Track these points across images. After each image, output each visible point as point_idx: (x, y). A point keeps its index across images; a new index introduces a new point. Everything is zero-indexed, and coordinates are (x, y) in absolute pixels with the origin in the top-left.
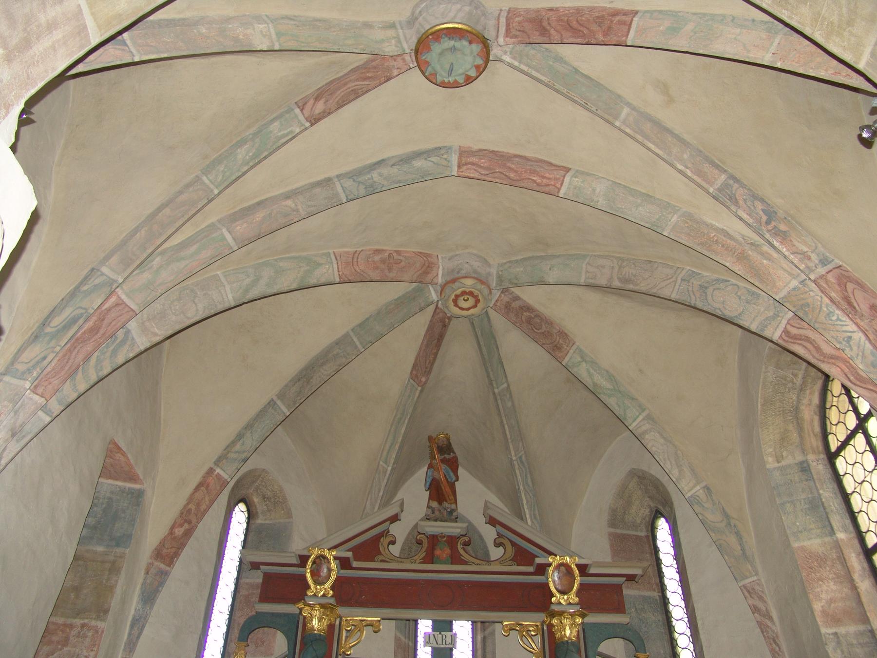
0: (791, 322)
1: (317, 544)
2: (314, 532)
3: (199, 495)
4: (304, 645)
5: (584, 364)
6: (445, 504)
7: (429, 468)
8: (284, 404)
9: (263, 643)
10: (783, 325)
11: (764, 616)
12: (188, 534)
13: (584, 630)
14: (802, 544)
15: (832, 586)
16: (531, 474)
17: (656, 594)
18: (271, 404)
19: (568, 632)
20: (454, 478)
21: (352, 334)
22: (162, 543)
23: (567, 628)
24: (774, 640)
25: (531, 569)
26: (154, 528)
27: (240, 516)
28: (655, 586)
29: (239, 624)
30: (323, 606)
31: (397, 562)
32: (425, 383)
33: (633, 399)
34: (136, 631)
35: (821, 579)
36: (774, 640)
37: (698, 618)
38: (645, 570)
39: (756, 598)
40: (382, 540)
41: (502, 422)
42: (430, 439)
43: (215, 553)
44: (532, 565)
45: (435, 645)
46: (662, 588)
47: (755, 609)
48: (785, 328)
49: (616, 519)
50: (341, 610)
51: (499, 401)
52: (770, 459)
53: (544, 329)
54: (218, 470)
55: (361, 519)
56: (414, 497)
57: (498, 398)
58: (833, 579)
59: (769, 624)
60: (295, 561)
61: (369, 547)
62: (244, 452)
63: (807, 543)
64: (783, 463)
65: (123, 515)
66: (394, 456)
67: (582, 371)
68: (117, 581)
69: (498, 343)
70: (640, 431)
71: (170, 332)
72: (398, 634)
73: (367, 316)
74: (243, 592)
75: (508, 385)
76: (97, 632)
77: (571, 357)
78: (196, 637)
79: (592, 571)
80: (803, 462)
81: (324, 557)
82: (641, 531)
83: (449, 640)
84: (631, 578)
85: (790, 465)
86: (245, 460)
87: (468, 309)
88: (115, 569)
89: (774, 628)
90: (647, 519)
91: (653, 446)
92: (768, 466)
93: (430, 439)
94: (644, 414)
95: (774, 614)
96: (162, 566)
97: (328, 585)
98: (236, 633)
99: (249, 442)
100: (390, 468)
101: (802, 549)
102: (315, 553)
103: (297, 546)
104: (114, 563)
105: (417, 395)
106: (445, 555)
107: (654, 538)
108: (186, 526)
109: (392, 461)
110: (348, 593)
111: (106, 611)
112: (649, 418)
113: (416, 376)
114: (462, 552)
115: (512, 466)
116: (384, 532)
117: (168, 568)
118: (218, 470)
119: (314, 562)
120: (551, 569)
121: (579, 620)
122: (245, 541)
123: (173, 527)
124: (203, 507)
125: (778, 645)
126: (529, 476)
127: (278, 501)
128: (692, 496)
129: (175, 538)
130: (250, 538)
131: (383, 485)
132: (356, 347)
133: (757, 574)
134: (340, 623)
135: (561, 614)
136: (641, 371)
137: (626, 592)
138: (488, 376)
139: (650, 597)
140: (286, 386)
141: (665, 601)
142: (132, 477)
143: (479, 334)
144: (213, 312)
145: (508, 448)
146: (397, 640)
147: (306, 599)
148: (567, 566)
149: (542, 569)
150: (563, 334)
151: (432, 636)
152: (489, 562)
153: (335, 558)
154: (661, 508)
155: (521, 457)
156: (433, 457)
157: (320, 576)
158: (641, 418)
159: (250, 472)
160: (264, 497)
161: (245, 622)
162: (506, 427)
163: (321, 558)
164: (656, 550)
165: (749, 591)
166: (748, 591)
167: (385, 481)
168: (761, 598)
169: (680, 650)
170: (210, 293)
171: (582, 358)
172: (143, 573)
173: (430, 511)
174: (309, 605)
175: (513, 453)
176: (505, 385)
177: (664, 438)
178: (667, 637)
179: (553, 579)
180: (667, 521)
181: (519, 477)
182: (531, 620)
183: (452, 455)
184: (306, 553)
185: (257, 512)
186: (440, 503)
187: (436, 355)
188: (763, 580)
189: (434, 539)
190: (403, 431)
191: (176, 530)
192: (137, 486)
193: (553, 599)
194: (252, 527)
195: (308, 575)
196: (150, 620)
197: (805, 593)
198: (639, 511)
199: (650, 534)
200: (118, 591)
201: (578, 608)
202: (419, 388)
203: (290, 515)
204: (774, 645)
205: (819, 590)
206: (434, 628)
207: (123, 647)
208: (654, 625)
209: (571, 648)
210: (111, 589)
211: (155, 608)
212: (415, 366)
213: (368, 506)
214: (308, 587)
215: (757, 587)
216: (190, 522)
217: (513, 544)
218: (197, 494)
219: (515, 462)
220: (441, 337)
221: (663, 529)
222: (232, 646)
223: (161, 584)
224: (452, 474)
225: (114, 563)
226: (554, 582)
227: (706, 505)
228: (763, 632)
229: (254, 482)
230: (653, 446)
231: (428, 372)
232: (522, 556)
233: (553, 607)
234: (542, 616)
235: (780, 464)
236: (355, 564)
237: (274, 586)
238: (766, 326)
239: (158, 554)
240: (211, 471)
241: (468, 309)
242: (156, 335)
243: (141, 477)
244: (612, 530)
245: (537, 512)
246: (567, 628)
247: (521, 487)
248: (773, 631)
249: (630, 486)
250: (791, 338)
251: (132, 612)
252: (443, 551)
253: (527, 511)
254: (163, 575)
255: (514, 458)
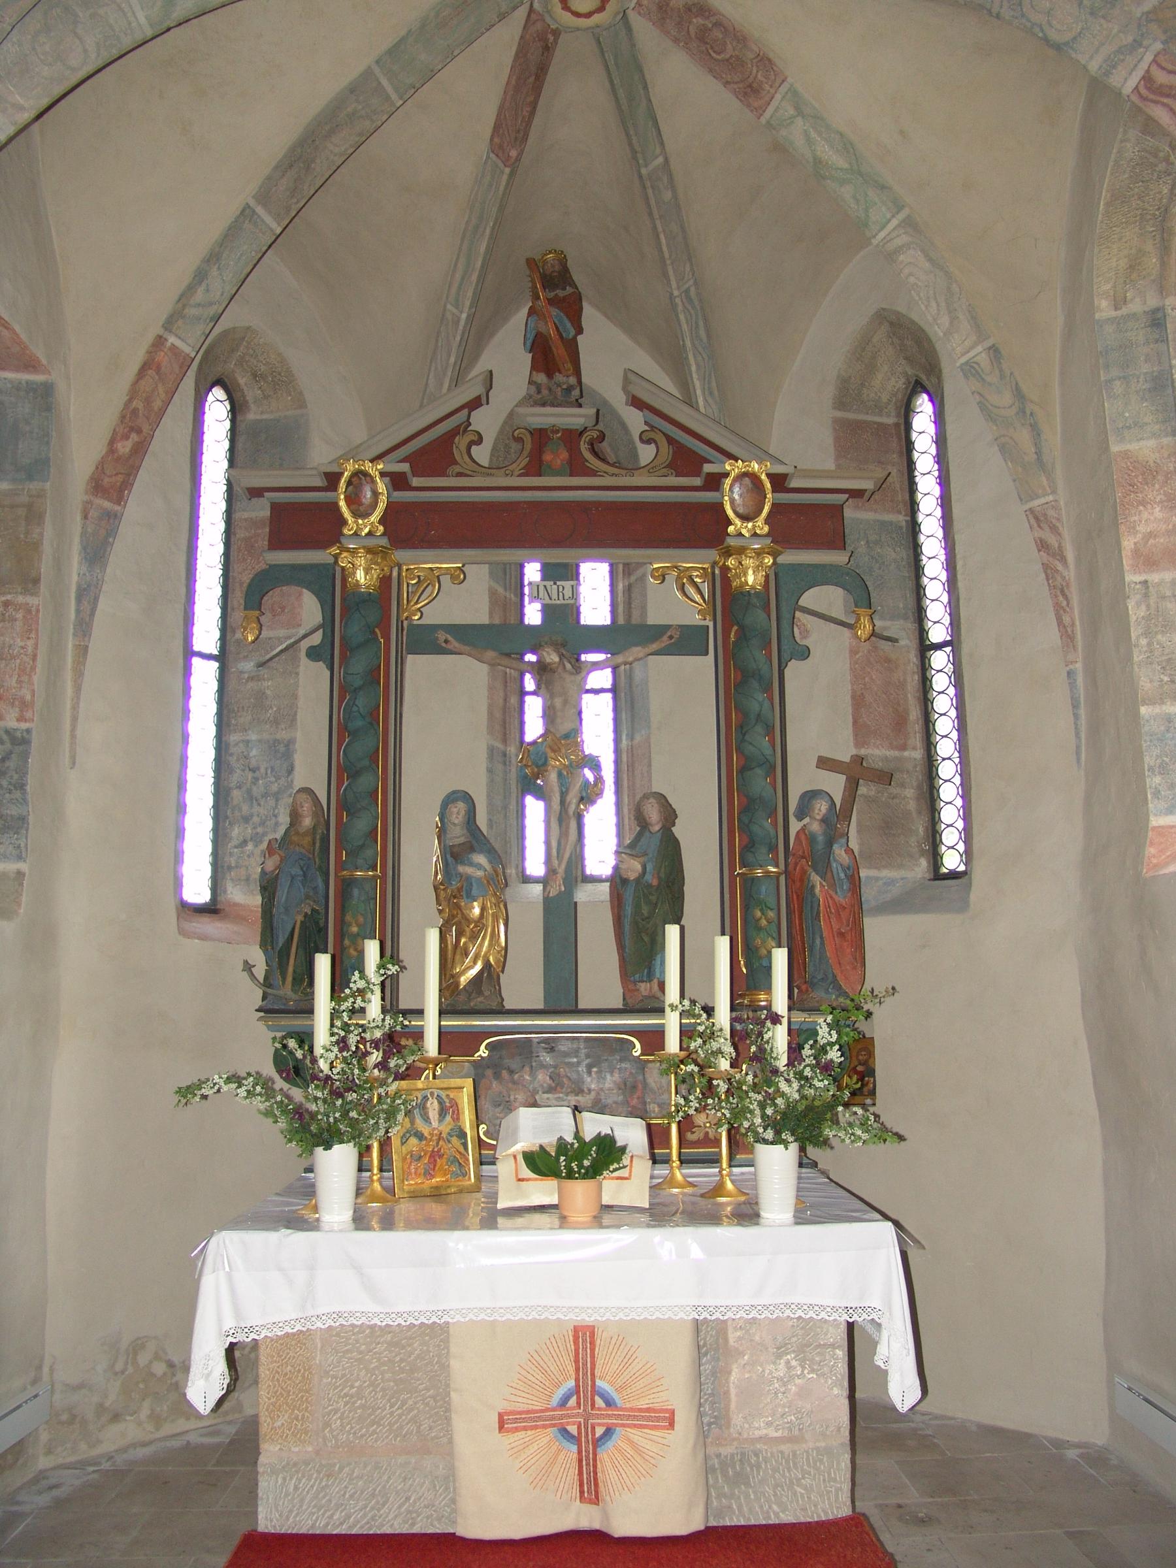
0: (1161, 59)
1: (352, 454)
2: (345, 432)
3: (146, 384)
4: (345, 610)
5: (799, 121)
6: (559, 377)
7: (530, 314)
8: (270, 213)
9: (283, 608)
10: (1144, 66)
11: (1054, 555)
12: (140, 450)
13: (776, 575)
14: (1129, 447)
15: (1158, 512)
16: (706, 320)
17: (902, 519)
18: (246, 213)
19: (751, 579)
20: (572, 332)
21: (377, 70)
22: (100, 467)
23: (750, 572)
24: (1062, 591)
25: (697, 481)
26: (83, 446)
27: (217, 410)
28: (901, 506)
29: (241, 584)
30: (369, 551)
31: (486, 473)
32: (518, 159)
33: (883, 187)
34: (86, 605)
35: (1143, 503)
36: (1062, 591)
37: (958, 557)
38: (881, 485)
39: (1047, 529)
40: (456, 440)
41: (655, 227)
42: (531, 263)
43: (188, 475)
44: (698, 475)
45: (547, 601)
46: (913, 507)
47: (1042, 545)
48: (1148, 71)
49: (847, 394)
50: (400, 555)
51: (650, 191)
52: (1104, 304)
53: (729, 51)
54: (172, 340)
55: (421, 406)
56: (508, 360)
57: (648, 184)
58: (1161, 502)
59: (1060, 567)
60: (319, 482)
61: (436, 453)
62: (211, 304)
63: (1133, 447)
64: (1124, 311)
65: (28, 428)
66: (470, 294)
67: (796, 133)
68: (41, 534)
69: (647, 77)
70: (890, 247)
71: (45, 102)
72: (493, 584)
73: (403, 33)
74: (241, 534)
75: (666, 160)
76: (29, 611)
77: (779, 105)
78: (180, 608)
79: (794, 484)
80: (1158, 309)
81: (366, 474)
82: (888, 416)
83: (568, 593)
84: (856, 494)
85: (1135, 314)
86: (217, 319)
87: (588, 15)
88: (34, 515)
89: (1066, 574)
90: (900, 396)
91: (911, 274)
92: (1097, 316)
93: (531, 263)
94: (901, 216)
95: (1070, 556)
96: (107, 504)
97: (375, 517)
98: (238, 598)
99: (219, 284)
100: (464, 316)
101: (1126, 455)
102: (350, 468)
103: (321, 454)
104: (30, 506)
105: (504, 183)
106: (559, 462)
107: (908, 427)
108: (134, 437)
109: (468, 303)
110: (408, 527)
111: (36, 581)
112: (909, 224)
113: (501, 147)
114: (587, 455)
115: (674, 306)
116: (459, 426)
117: (117, 508)
118: (172, 340)
119: (349, 483)
120: (728, 481)
121: (769, 561)
122: (232, 450)
123: (112, 442)
124: (157, 404)
125: (1066, 598)
126: (701, 323)
127: (279, 380)
128: (967, 363)
129: (118, 459)
130: (240, 445)
131: (455, 345)
132: (388, 98)
133: (1054, 492)
134: (399, 574)
135: (741, 551)
136: (902, 132)
137: (848, 513)
138: (630, 144)
139: (891, 523)
140: (269, 178)
141: (914, 528)
142: (31, 365)
143: (611, 63)
144: (115, 53)
145: (665, 274)
146: (493, 593)
147: (343, 540)
148: (754, 478)
149: (714, 482)
150: (765, 61)
151: (542, 589)
152: (633, 468)
153: (383, 474)
154: (923, 377)
155: (687, 291)
156: (536, 297)
157: (360, 504)
158: (895, 222)
159: (225, 334)
160: (255, 375)
161: (253, 580)
162: (662, 236)
163: (360, 476)
164: (909, 446)
165: (1038, 518)
166: (1037, 519)
167: (458, 338)
168: (1054, 529)
169: (928, 602)
170: (101, 11)
171: (797, 108)
172: (79, 518)
173: (533, 389)
174: (348, 550)
175: (674, 284)
176: (661, 160)
177: (930, 260)
178: (911, 584)
179: (732, 496)
180: (931, 400)
181: (685, 326)
182: (696, 562)
183: (569, 290)
184: (334, 468)
185: (247, 402)
186: (550, 375)
187: (534, 106)
188: (1062, 503)
189: (541, 436)
190: (483, 249)
191: (119, 445)
192: (39, 378)
193: (731, 529)
194: (241, 427)
195: (342, 504)
196: (105, 588)
197: (1115, 524)
198: (888, 381)
199: (902, 421)
200: (47, 548)
201: (768, 541)
202: (507, 170)
203: (301, 404)
204: (1061, 598)
205: (1136, 518)
206: (544, 577)
207: (72, 631)
208: (893, 566)
209: (754, 600)
210: (36, 546)
211: (108, 570)
212: (497, 127)
213: (432, 381)
214: (344, 522)
215: (1051, 513)
216: (139, 431)
217: (671, 440)
218: (142, 382)
219: (678, 300)
220: (542, 71)
221: (924, 407)
222: (237, 616)
223: (112, 532)
224: (569, 325)
225: (30, 506)
226: (732, 501)
227: (988, 379)
228: (1048, 580)
229: (233, 351)
230: (911, 274)
231: (522, 137)
232: (684, 460)
233: (731, 542)
234: (713, 554)
235: (1119, 313)
236: (416, 482)
237: (288, 526)
238: (1114, 67)
239: (97, 486)
240: (159, 341)
241: (588, 15)
242: (21, 108)
243: (44, 361)
244: (839, 414)
245: (714, 384)
246: (750, 572)
247: (688, 343)
248: (1064, 578)
249: (875, 340)
250: (1153, 92)
251: (75, 578)
252: (556, 456)
253: (697, 384)
254: (112, 519)
255: (676, 293)
